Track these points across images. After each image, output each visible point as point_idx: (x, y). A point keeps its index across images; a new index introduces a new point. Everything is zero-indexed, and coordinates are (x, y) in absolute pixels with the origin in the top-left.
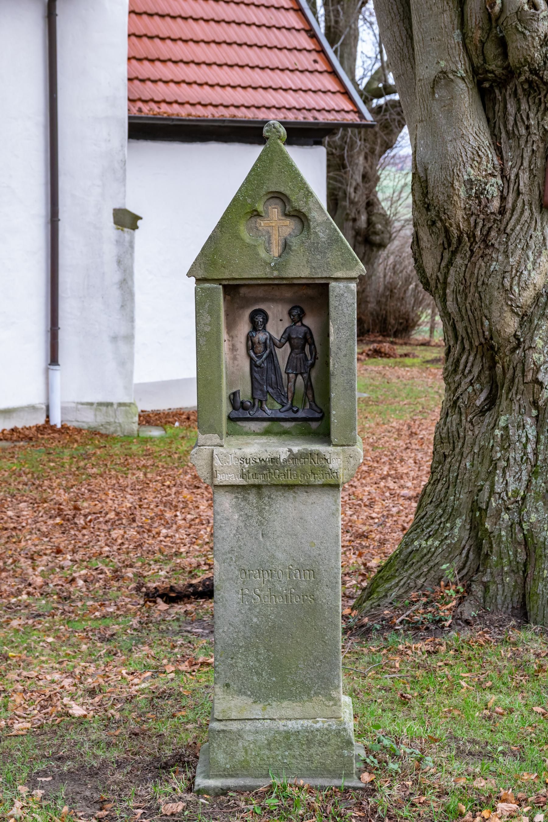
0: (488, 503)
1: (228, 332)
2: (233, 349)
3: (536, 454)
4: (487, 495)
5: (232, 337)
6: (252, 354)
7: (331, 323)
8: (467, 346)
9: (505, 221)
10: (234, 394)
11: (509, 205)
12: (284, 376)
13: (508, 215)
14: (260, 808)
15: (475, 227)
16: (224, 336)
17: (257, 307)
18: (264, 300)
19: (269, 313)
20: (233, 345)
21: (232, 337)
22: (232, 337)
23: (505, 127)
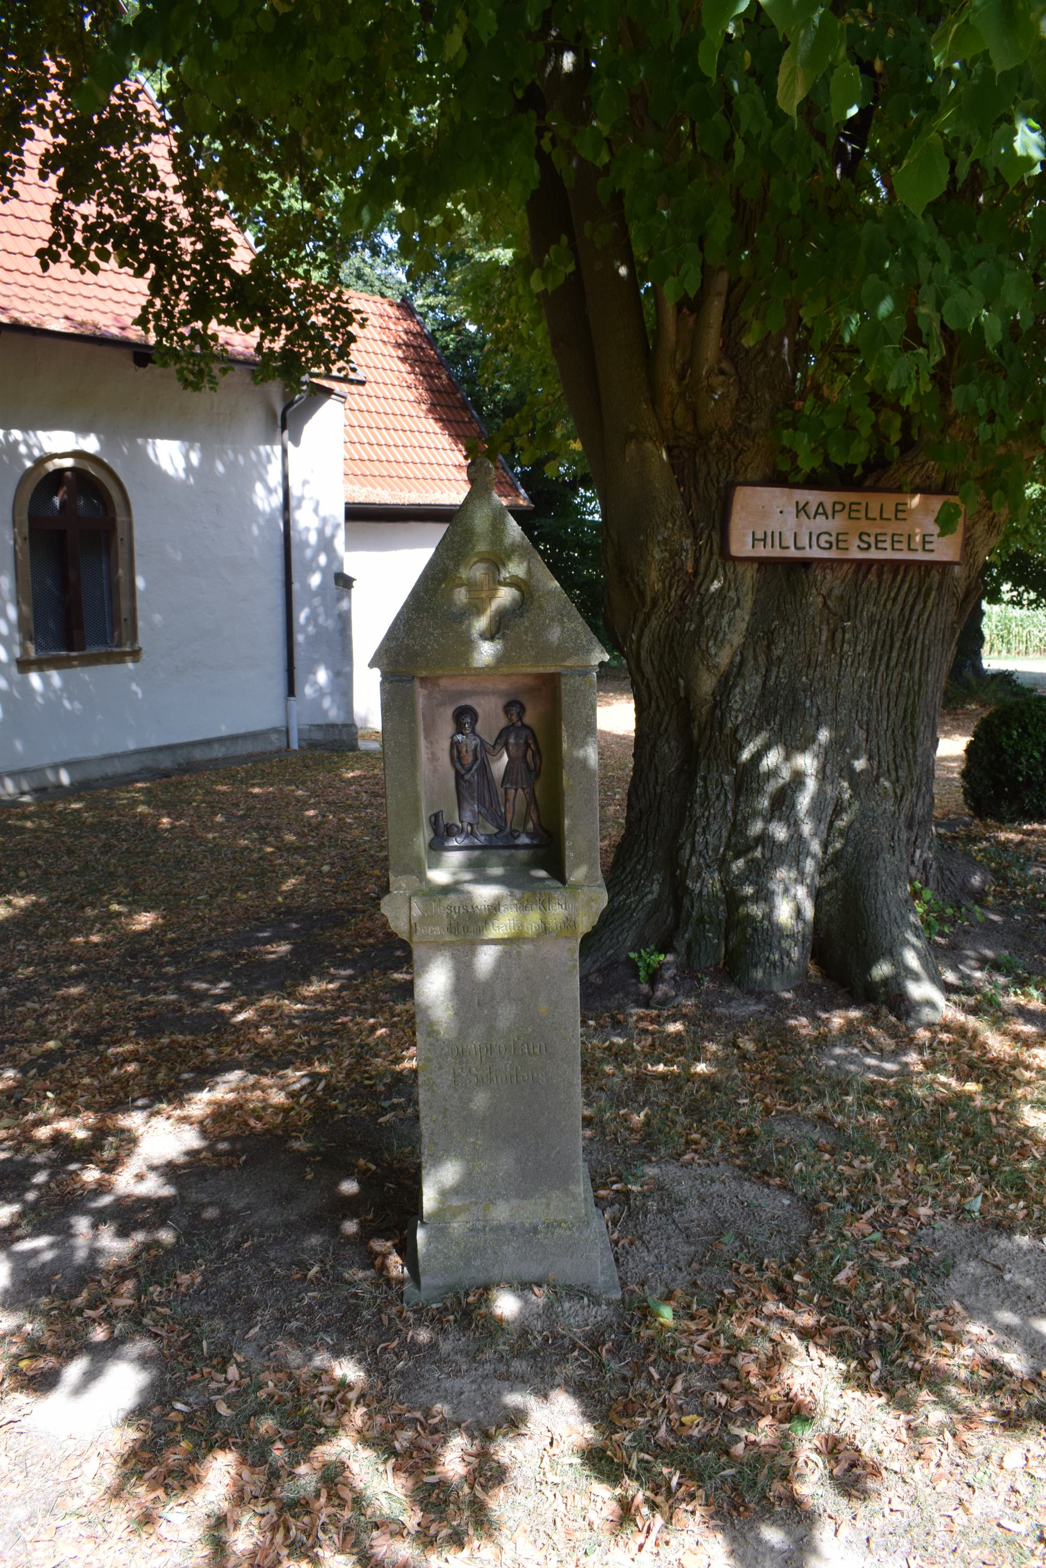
0: (689, 860)
1: (426, 738)
2: (433, 758)
3: (735, 814)
4: (688, 851)
5: (431, 743)
6: (459, 767)
7: (565, 736)
8: (662, 706)
9: (698, 581)
10: (436, 816)
11: (702, 569)
12: (501, 791)
13: (700, 577)
14: (506, 1450)
15: (670, 589)
16: (423, 743)
17: (463, 703)
18: (472, 693)
19: (479, 711)
20: (433, 754)
21: (431, 743)
22: (431, 743)
23: (696, 490)
